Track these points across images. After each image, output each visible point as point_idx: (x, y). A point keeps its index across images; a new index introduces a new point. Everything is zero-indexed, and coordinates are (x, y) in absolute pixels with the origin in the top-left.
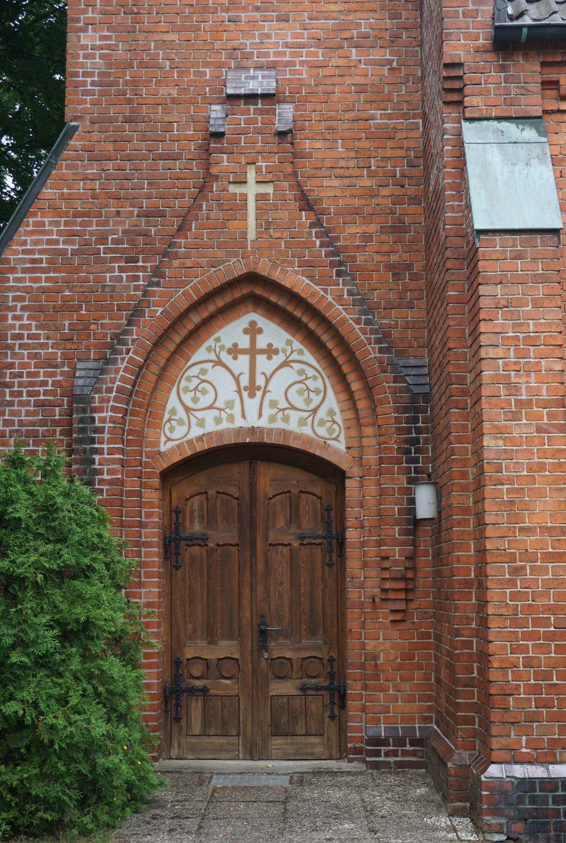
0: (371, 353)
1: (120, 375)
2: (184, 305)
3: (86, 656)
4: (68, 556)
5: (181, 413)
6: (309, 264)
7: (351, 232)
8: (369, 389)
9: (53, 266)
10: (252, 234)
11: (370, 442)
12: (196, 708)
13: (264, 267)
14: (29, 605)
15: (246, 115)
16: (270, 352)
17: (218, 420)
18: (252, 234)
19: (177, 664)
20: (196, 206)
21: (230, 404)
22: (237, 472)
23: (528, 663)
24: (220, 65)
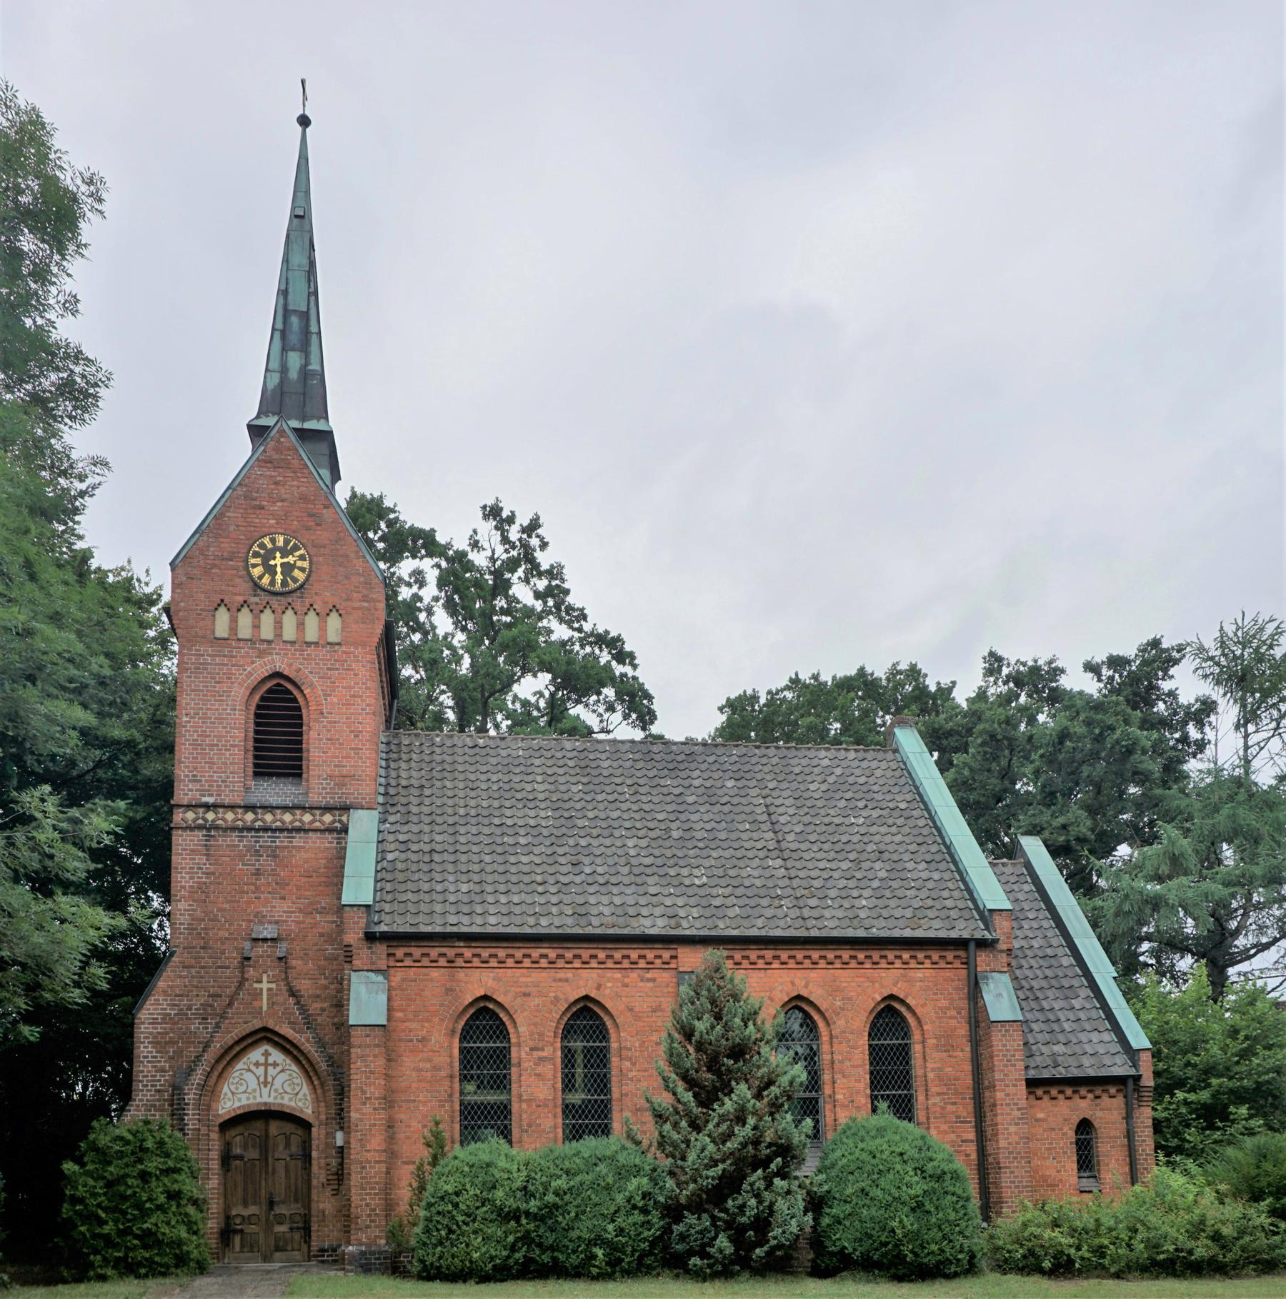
0: (323, 1066)
1: (198, 1077)
2: (230, 1043)
3: (179, 1205)
4: (171, 1163)
5: (230, 1095)
6: (293, 1023)
7: (315, 1007)
8: (322, 1085)
9: (164, 1021)
10: (265, 1008)
11: (323, 1109)
12: (237, 1239)
13: (271, 1024)
14: (154, 1183)
15: (261, 949)
16: (275, 1065)
17: (248, 1099)
18: (265, 1008)
19: (228, 1218)
20: (236, 993)
21: (254, 1091)
22: (259, 1125)
23: (367, 1205)
24: (250, 921)
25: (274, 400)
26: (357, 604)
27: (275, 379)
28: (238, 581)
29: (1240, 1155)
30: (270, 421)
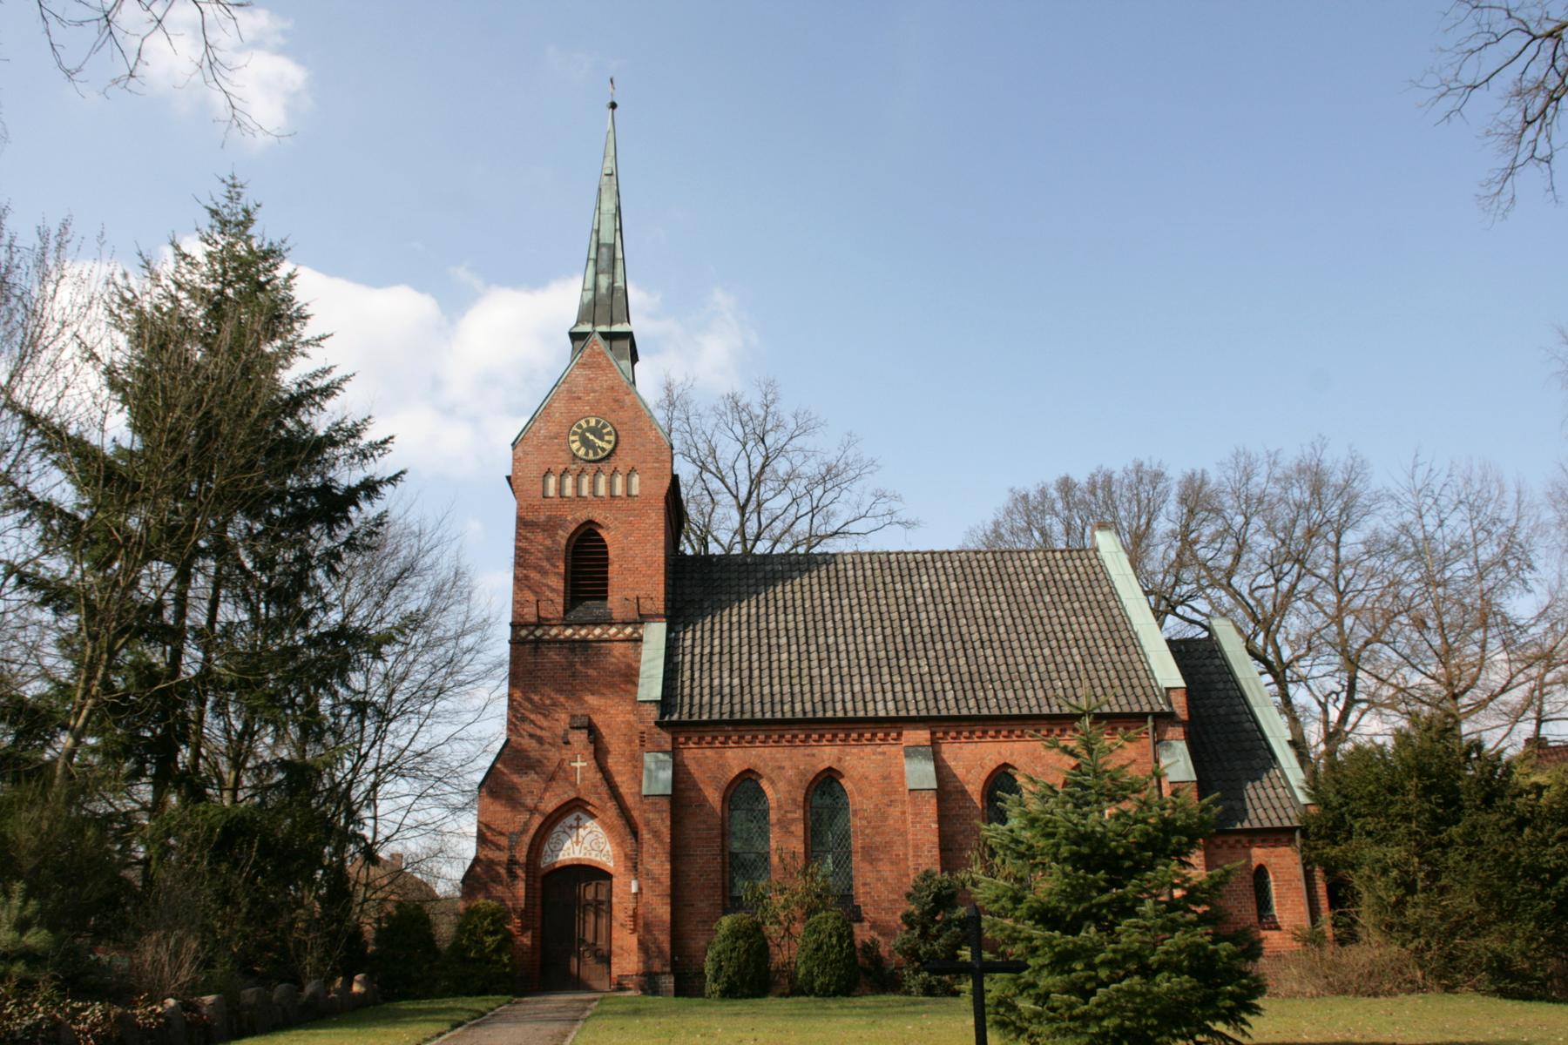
25: (590, 311)
27: (590, 295)
29: (263, 611)
30: (587, 328)
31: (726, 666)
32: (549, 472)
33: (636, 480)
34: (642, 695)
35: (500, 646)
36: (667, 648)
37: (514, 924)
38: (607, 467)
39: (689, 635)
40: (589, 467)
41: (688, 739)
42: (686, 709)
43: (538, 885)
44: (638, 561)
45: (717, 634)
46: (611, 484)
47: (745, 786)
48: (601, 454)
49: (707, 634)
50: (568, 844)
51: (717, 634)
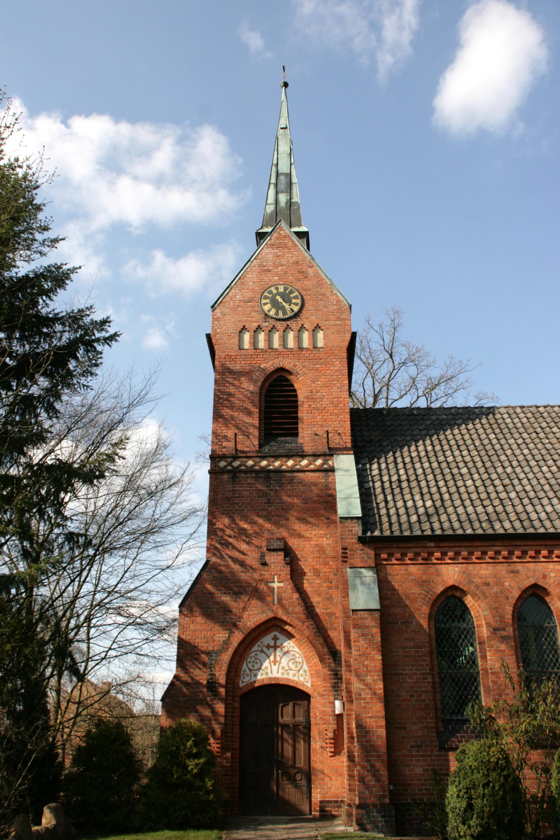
5: (248, 671)
26: (332, 323)
27: (270, 209)
28: (254, 314)
31: (416, 491)
32: (244, 329)
33: (320, 335)
34: (341, 511)
35: (196, 490)
36: (359, 476)
37: (214, 745)
38: (293, 324)
39: (375, 466)
40: (279, 325)
41: (391, 555)
42: (386, 526)
43: (237, 705)
44: (325, 402)
45: (401, 466)
46: (299, 339)
47: (451, 605)
48: (289, 314)
49: (391, 466)
50: (266, 664)
51: (401, 466)
